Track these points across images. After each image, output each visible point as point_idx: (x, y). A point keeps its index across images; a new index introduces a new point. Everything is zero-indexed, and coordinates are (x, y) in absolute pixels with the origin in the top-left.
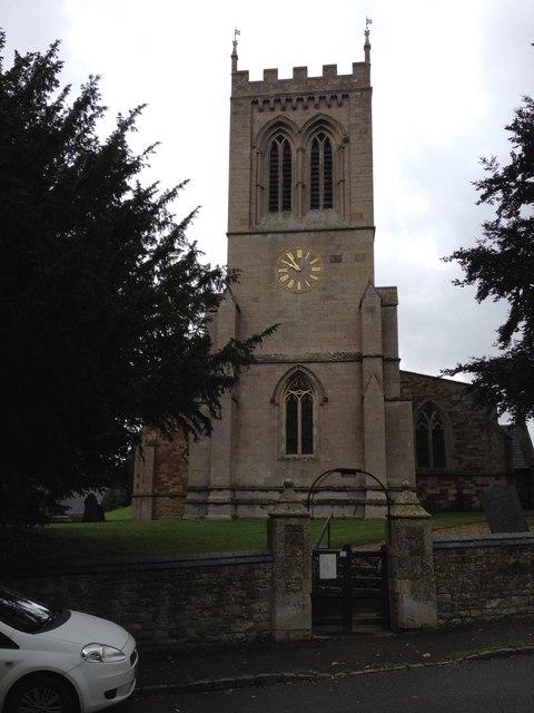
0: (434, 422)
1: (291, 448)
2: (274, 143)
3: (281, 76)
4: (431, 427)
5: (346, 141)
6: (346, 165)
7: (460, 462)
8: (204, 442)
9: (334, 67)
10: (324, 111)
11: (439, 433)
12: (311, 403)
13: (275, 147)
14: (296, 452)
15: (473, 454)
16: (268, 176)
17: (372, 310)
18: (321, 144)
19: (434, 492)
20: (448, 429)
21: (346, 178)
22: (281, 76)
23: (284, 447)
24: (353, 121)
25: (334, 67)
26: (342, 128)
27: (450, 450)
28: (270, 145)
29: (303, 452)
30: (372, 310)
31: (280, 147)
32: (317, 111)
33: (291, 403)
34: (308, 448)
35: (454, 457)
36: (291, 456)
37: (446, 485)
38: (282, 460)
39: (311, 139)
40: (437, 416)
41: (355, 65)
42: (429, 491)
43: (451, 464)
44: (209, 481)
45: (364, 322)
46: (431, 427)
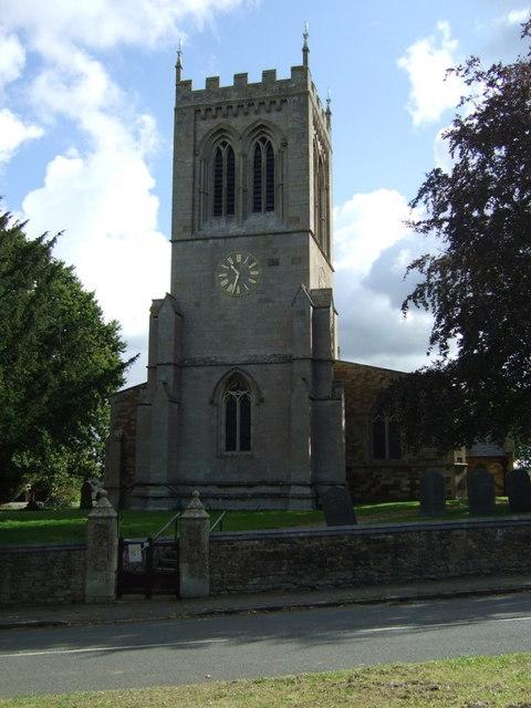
1: (230, 445)
3: (222, 84)
5: (285, 145)
13: (219, 152)
14: (234, 449)
19: (388, 482)
22: (222, 84)
23: (223, 444)
31: (224, 151)
33: (231, 403)
34: (246, 446)
38: (221, 457)
41: (294, 69)
42: (383, 482)
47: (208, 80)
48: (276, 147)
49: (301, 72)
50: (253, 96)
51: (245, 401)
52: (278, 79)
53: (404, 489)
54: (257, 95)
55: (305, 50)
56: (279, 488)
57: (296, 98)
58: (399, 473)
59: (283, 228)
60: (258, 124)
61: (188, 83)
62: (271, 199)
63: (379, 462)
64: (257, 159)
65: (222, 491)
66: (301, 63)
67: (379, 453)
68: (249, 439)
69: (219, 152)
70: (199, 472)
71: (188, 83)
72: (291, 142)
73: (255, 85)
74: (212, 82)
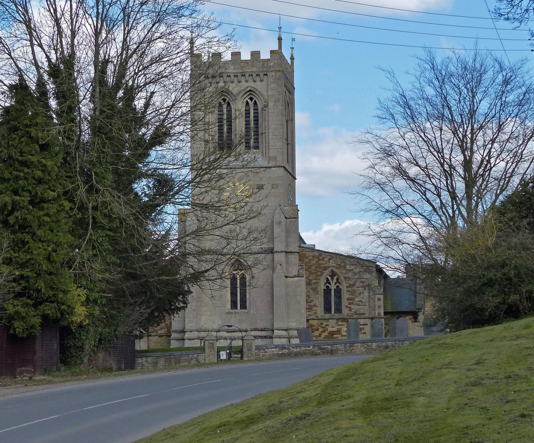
0: (336, 283)
1: (234, 305)
2: (220, 103)
3: (263, 57)
4: (333, 287)
5: (266, 106)
6: (266, 122)
7: (350, 310)
8: (58, 373)
9: (258, 53)
10: (251, 84)
11: (338, 291)
12: (246, 278)
13: (247, 103)
14: (236, 308)
15: (358, 305)
16: (259, 120)
17: (279, 223)
18: (251, 103)
19: (333, 329)
20: (344, 287)
21: (267, 132)
22: (263, 57)
23: (229, 305)
24: (270, 93)
25: (258, 53)
26: (262, 95)
27: (345, 302)
28: (245, 103)
29: (241, 309)
30: (279, 223)
31: (251, 103)
32: (247, 84)
33: (233, 279)
34: (244, 306)
35: (347, 307)
36: (234, 311)
37: (340, 325)
38: (228, 313)
39: (245, 101)
40: (337, 280)
41: (272, 52)
42: (330, 329)
43: (345, 311)
44: (287, 258)
45: (275, 230)
46: (333, 287)
47: (233, 54)
48: (260, 107)
49: (276, 54)
50: (245, 70)
51: (243, 278)
52: (261, 58)
53: (343, 334)
54: (248, 70)
55: (280, 39)
56: (265, 332)
57: (274, 73)
58: (340, 323)
59: (265, 164)
60: (248, 89)
61: (199, 56)
62: (257, 140)
63: (327, 316)
64: (247, 112)
65: (229, 334)
66: (276, 48)
67: (327, 310)
68: (246, 301)
69: (247, 103)
70: (214, 323)
71: (199, 56)
72: (270, 104)
73: (246, 61)
74: (255, 54)
